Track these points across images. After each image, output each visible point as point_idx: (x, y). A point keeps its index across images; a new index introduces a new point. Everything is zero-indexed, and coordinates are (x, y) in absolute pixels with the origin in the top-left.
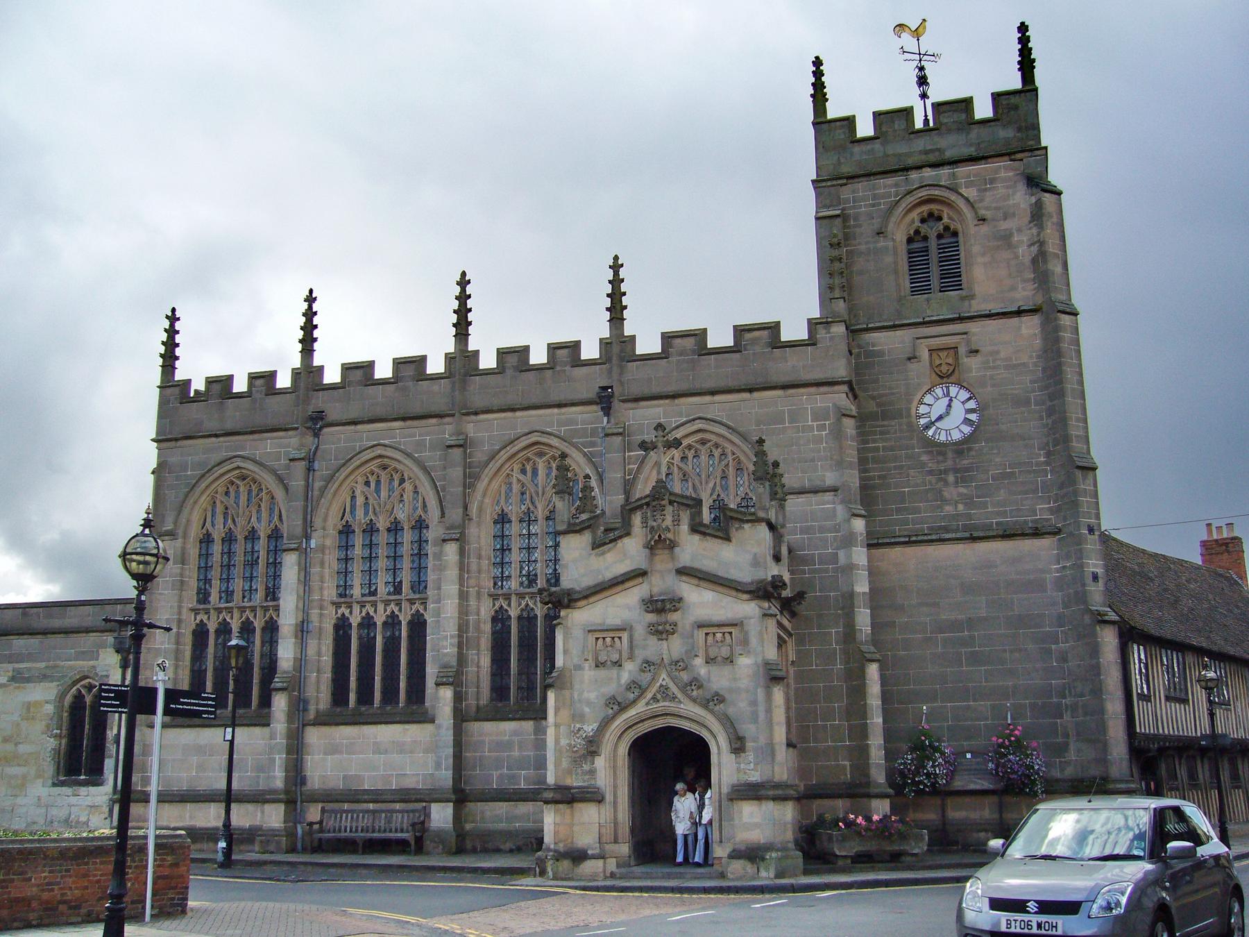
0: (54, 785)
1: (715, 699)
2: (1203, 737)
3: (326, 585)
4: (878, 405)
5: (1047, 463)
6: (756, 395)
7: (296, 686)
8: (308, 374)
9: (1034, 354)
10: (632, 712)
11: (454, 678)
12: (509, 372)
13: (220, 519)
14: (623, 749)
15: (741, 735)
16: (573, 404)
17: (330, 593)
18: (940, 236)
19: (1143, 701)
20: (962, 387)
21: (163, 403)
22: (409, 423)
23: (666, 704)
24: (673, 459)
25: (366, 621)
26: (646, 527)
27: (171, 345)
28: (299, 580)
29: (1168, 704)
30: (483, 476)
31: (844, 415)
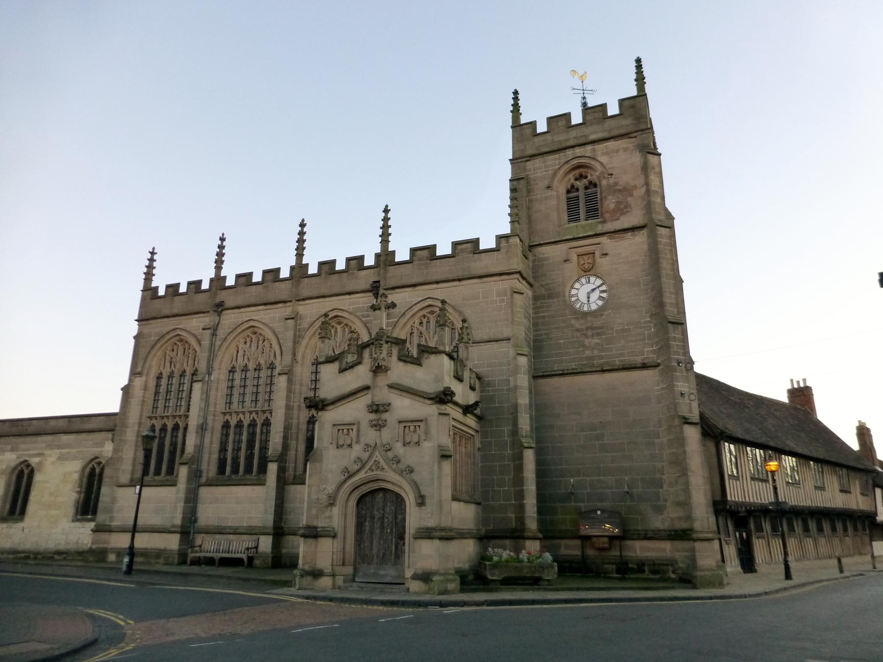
0: (73, 521)
1: (407, 469)
2: (771, 504)
3: (218, 402)
4: (546, 290)
5: (650, 322)
6: (463, 282)
7: (194, 463)
8: (385, 257)
9: (643, 254)
10: (356, 478)
11: (282, 459)
12: (323, 275)
13: (168, 364)
14: (353, 502)
15: (422, 494)
16: (357, 293)
17: (221, 406)
18: (586, 188)
19: (733, 480)
20: (598, 277)
21: (143, 299)
22: (268, 307)
23: (378, 472)
24: (414, 323)
25: (252, 423)
26: (371, 358)
27: (150, 267)
28: (201, 398)
29: (753, 482)
30: (305, 337)
31: (515, 292)
